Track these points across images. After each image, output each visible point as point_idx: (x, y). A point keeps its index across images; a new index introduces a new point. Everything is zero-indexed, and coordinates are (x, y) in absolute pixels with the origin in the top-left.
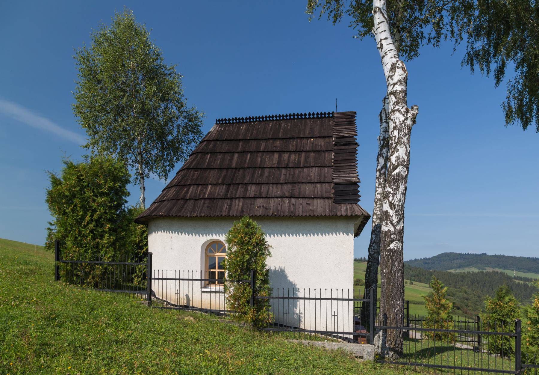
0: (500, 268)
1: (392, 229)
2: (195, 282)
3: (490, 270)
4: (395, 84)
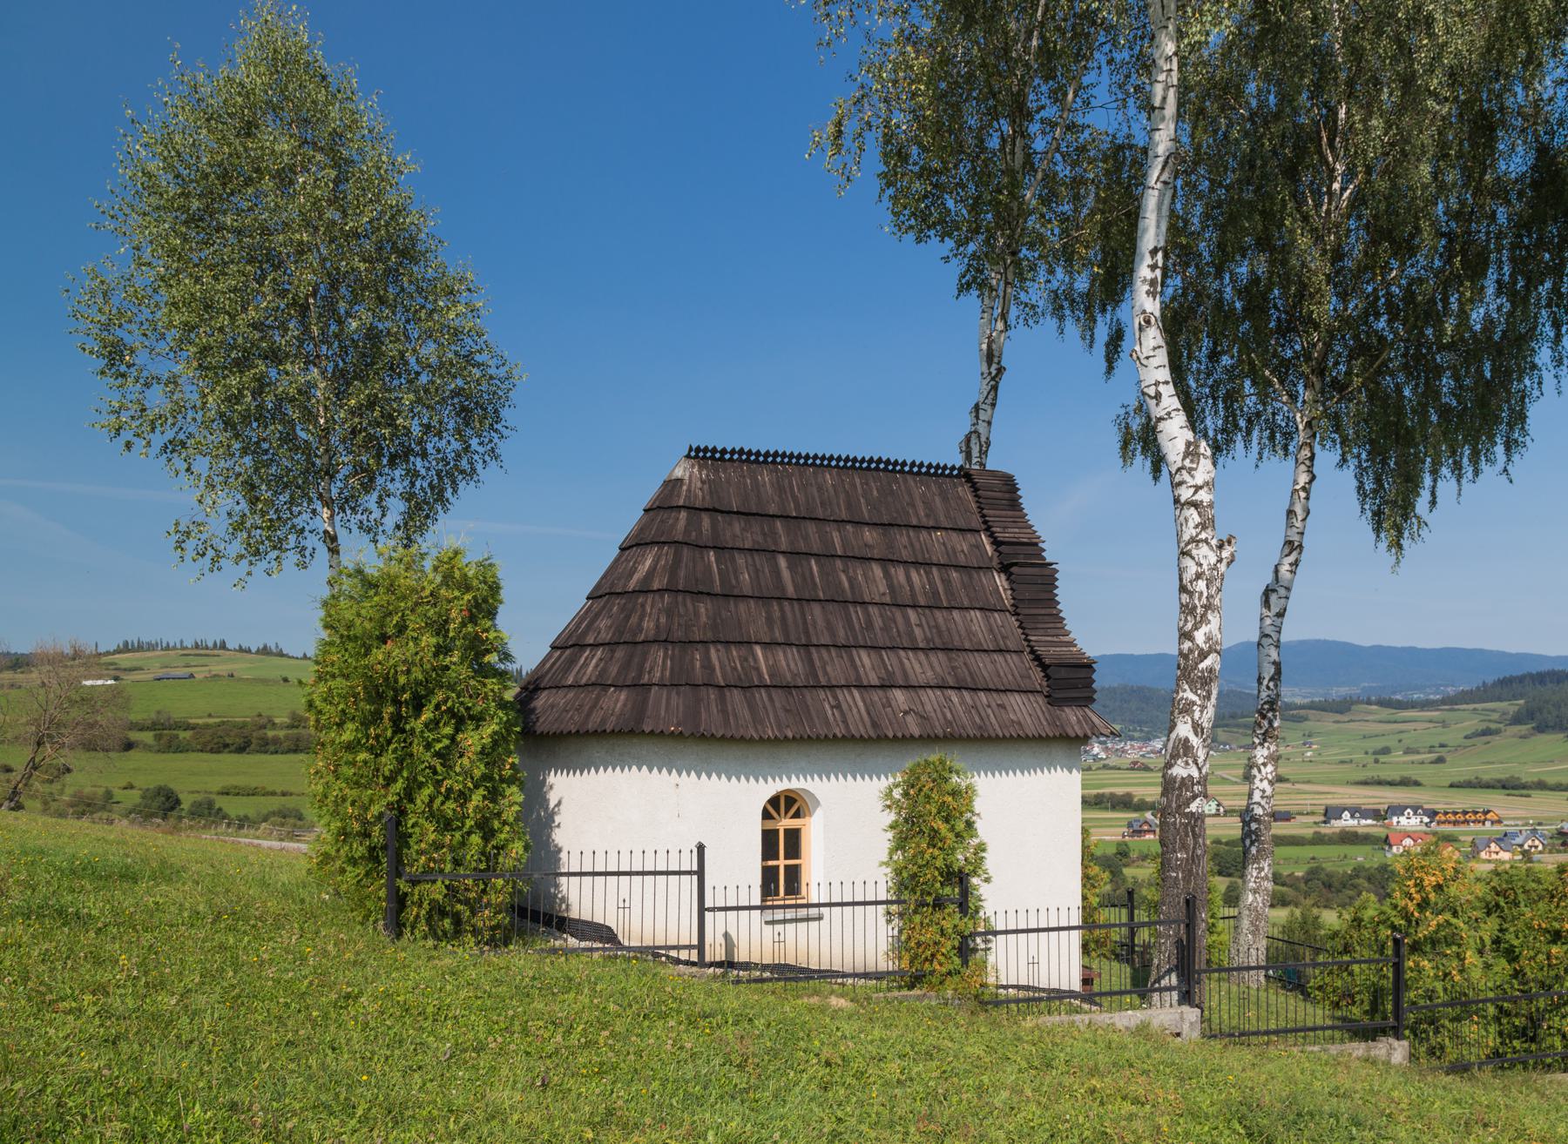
1: (1196, 774)
4: (1198, 488)
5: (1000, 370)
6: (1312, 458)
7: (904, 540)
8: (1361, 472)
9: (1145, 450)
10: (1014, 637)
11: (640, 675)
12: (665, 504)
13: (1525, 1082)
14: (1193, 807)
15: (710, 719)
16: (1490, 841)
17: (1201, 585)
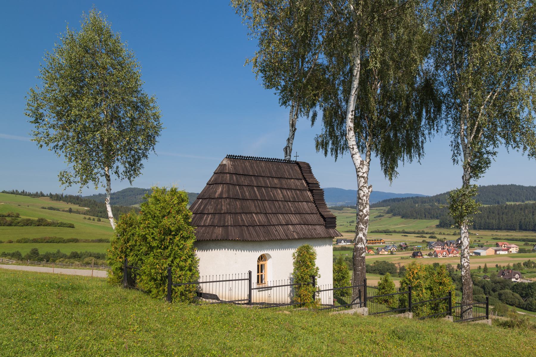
2: (286, 287)
4: (364, 173)
5: (295, 129)
6: (370, 155)
7: (284, 182)
8: (382, 159)
9: (322, 147)
10: (315, 210)
11: (225, 223)
12: (221, 171)
13: (437, 321)
14: (363, 255)
15: (247, 236)
16: (382, 249)
17: (365, 198)
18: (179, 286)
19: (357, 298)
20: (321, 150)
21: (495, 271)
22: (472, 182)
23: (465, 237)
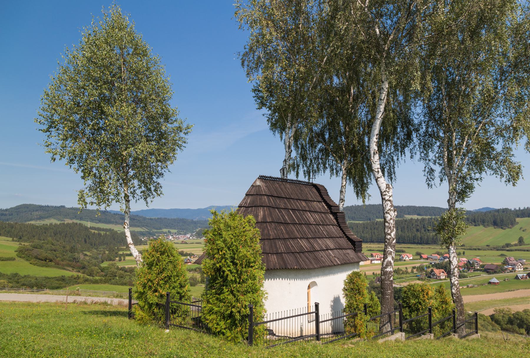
0: (77, 219)
3: (68, 221)
4: (390, 197)
17: (392, 221)
18: (246, 324)
19: (388, 322)
20: (292, 172)
21: (372, 278)
22: (458, 205)
23: (454, 256)
